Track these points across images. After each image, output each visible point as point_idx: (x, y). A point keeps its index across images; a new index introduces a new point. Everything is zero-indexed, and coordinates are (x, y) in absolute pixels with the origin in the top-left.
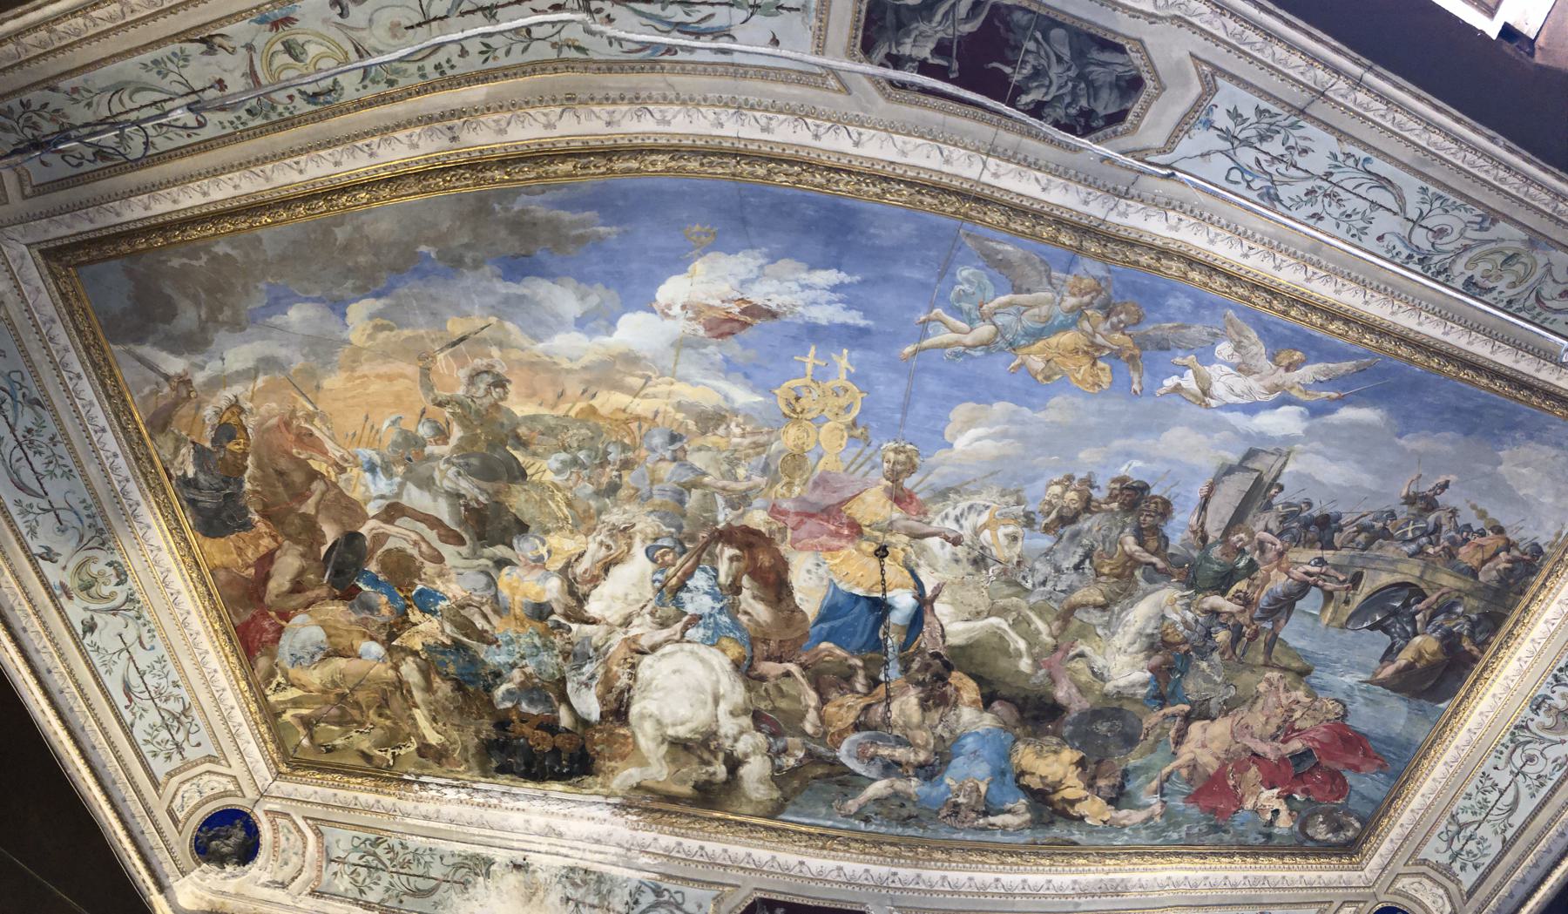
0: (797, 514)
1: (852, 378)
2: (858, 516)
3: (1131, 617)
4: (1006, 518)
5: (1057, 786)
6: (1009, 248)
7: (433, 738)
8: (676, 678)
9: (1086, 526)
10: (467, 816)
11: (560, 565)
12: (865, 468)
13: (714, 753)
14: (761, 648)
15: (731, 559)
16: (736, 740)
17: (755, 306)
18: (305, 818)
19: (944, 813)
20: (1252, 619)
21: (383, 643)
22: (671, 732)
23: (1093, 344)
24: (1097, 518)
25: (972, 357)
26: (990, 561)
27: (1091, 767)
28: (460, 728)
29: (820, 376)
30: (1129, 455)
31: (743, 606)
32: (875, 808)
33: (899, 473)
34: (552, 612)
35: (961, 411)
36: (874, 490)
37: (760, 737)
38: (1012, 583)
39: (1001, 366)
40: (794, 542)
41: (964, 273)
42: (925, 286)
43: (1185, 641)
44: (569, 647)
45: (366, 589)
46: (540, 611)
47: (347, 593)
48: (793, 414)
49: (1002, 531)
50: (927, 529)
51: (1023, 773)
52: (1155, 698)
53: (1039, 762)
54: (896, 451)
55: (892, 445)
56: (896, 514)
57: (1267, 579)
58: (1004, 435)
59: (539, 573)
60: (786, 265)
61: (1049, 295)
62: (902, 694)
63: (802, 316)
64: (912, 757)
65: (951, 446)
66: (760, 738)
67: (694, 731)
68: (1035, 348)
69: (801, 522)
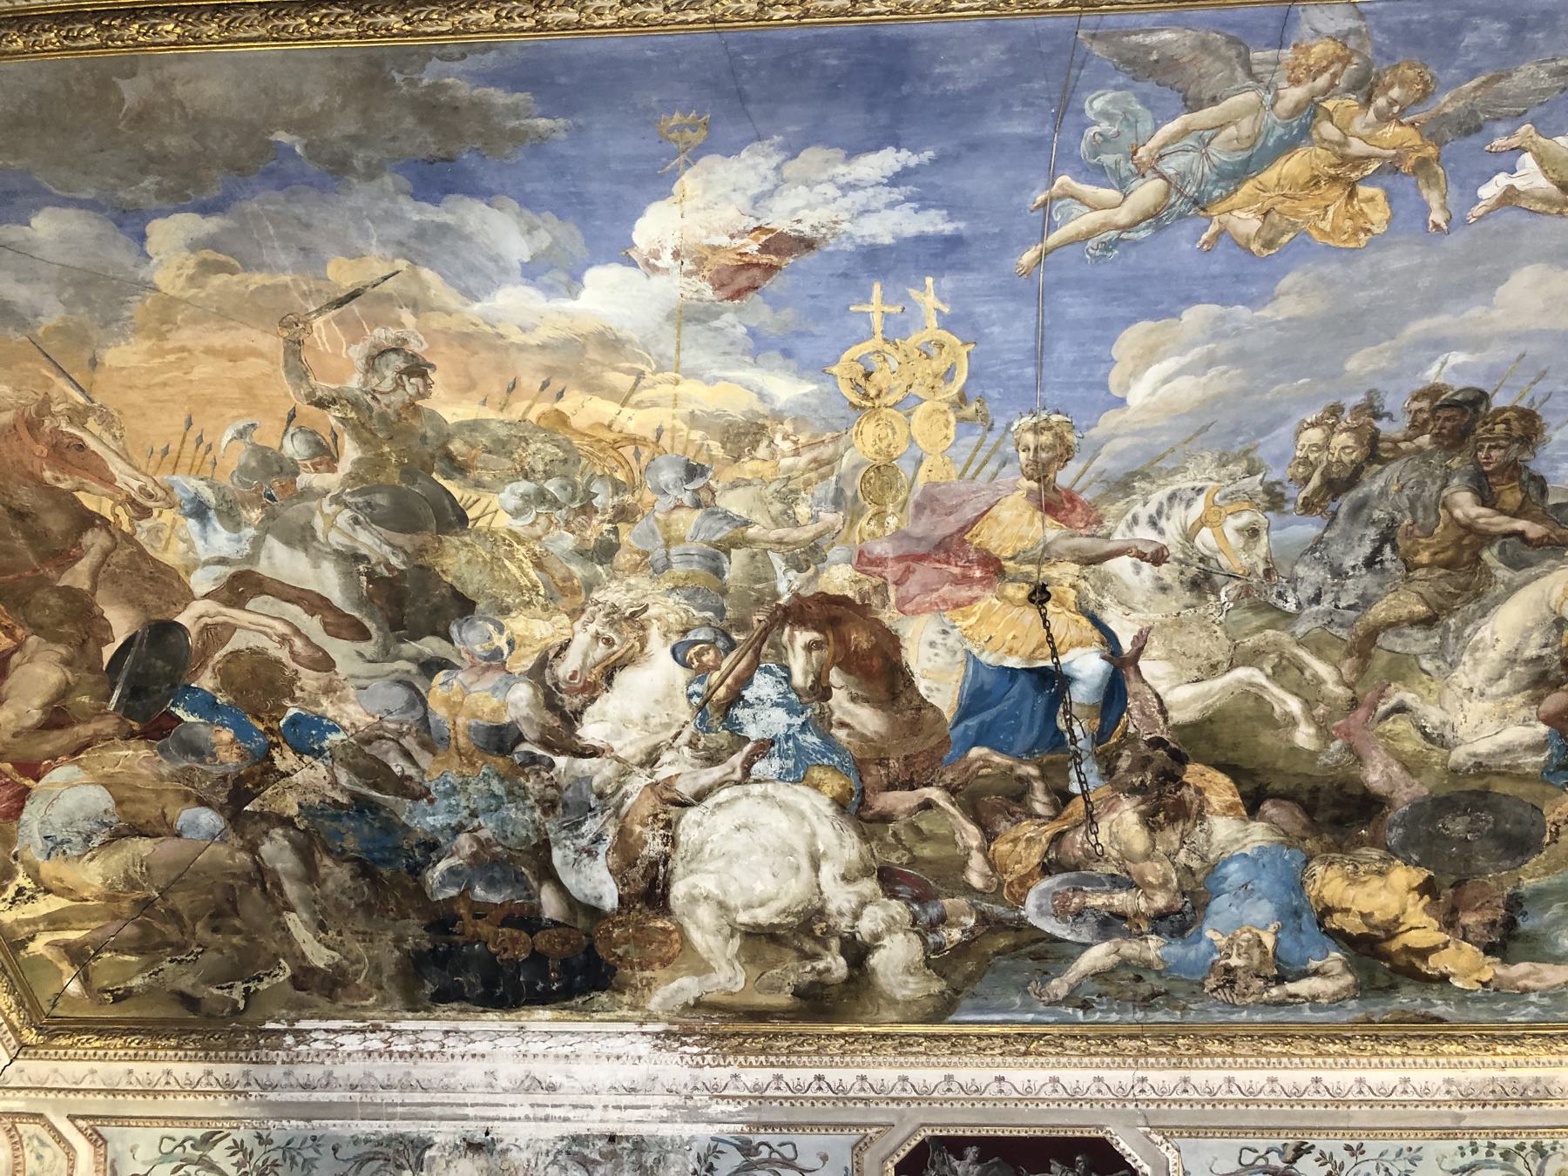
0: (899, 559)
2: (993, 546)
3: (1485, 633)
5: (1392, 928)
7: (320, 956)
8: (743, 836)
9: (1375, 488)
10: (380, 1076)
11: (528, 663)
12: (991, 467)
13: (823, 941)
14: (876, 773)
15: (808, 648)
16: (857, 916)
17: (781, 236)
18: (72, 1118)
19: (1211, 983)
21: (220, 809)
22: (743, 918)
24: (1393, 470)
25: (1136, 243)
26: (1218, 578)
28: (367, 938)
29: (896, 330)
30: (1439, 345)
31: (837, 715)
32: (1096, 987)
33: (1046, 465)
34: (521, 739)
39: (1185, 243)
40: (901, 603)
41: (1097, 103)
42: (1037, 144)
44: (551, 792)
45: (189, 718)
46: (500, 739)
47: (154, 727)
48: (866, 402)
49: (1231, 524)
50: (1109, 547)
51: (1328, 911)
53: (1352, 892)
54: (1036, 430)
55: (1028, 421)
56: (1052, 531)
58: (1210, 362)
59: (494, 678)
60: (812, 157)
61: (1251, 96)
62: (1111, 809)
63: (850, 237)
64: (1142, 904)
65: (1122, 402)
67: (784, 912)
68: (1237, 198)
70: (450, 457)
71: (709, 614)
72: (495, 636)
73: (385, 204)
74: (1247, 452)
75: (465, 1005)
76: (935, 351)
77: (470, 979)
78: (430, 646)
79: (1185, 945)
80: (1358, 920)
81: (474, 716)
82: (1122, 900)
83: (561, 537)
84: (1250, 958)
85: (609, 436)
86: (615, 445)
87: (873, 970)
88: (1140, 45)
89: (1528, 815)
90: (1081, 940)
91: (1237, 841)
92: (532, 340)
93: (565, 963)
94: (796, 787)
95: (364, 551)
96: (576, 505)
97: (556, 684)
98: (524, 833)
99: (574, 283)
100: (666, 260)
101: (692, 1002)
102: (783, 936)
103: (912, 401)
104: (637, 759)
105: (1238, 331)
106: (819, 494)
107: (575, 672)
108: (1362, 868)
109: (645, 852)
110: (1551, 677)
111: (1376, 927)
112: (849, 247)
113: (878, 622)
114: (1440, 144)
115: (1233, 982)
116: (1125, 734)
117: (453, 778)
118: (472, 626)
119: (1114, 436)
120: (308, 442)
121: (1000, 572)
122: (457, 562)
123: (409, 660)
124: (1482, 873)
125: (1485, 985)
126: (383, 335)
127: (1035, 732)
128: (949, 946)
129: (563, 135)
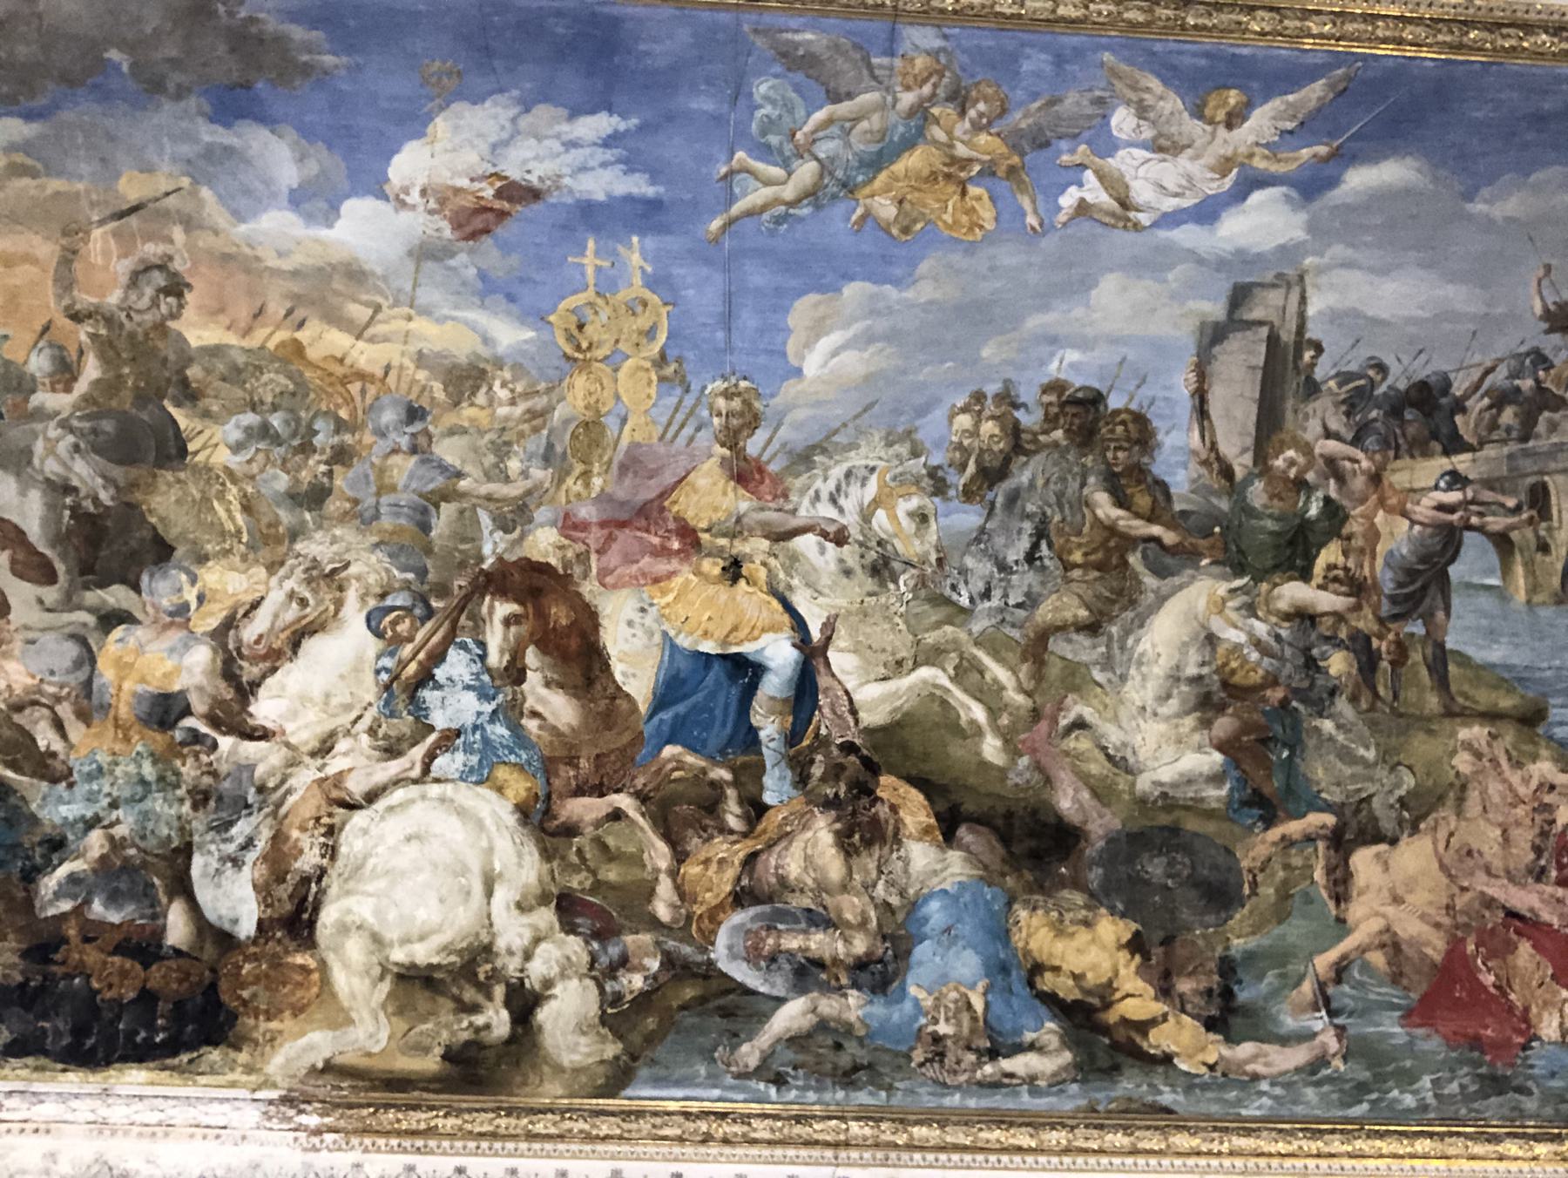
0: (603, 524)
1: (652, 283)
2: (689, 515)
3: (1145, 645)
4: (906, 484)
5: (1107, 993)
6: (809, 36)
8: (413, 849)
9: (1025, 478)
11: (213, 623)
12: (688, 431)
13: (485, 989)
15: (507, 622)
16: (528, 956)
19: (918, 1056)
20: (1381, 621)
22: (398, 955)
23: (954, 161)
24: (1039, 459)
25: (801, 220)
26: (896, 565)
27: (1157, 952)
29: (607, 285)
32: (790, 1055)
34: (187, 711)
35: (802, 311)
36: (706, 466)
37: (574, 945)
38: (940, 601)
39: (839, 221)
42: (718, 120)
43: (1272, 680)
46: (165, 710)
48: (578, 358)
49: (904, 506)
50: (794, 523)
51: (1037, 969)
52: (1245, 803)
53: (1059, 946)
54: (728, 395)
56: (744, 503)
57: (1373, 535)
58: (868, 339)
59: (175, 636)
60: (543, 112)
63: (571, 191)
65: (798, 372)
66: (574, 946)
67: (446, 949)
69: (610, 538)
70: (185, 382)
71: (410, 576)
72: (186, 587)
73: (184, 124)
74: (909, 433)
75: (43, 1061)
76: (639, 309)
77: (57, 1026)
78: (116, 596)
79: (889, 1003)
80: (1071, 982)
81: (143, 680)
82: (819, 943)
83: (275, 477)
84: (959, 1024)
85: (339, 371)
86: (344, 381)
87: (540, 1028)
88: (788, 41)
89: (1221, 859)
90: (775, 993)
91: (935, 873)
92: (286, 265)
93: (179, 1005)
94: (479, 789)
95: (75, 482)
96: (296, 442)
97: (238, 650)
98: (165, 831)
99: (331, 214)
100: (414, 197)
101: (320, 1065)
102: (442, 981)
103: (618, 358)
104: (309, 747)
105: (890, 311)
106: (531, 447)
107: (261, 636)
108: (1068, 916)
109: (297, 865)
110: (1215, 699)
111: (1088, 992)
112: (570, 201)
113: (579, 595)
114: (1022, 154)
115: (942, 1055)
116: (817, 735)
117: (103, 758)
118: (165, 576)
119: (795, 406)
120: (53, 358)
121: (697, 544)
122: (167, 503)
123: (90, 610)
124: (1190, 929)
125: (1212, 1068)
126: (152, 250)
127: (729, 725)
128: (629, 997)
129: (343, 72)
